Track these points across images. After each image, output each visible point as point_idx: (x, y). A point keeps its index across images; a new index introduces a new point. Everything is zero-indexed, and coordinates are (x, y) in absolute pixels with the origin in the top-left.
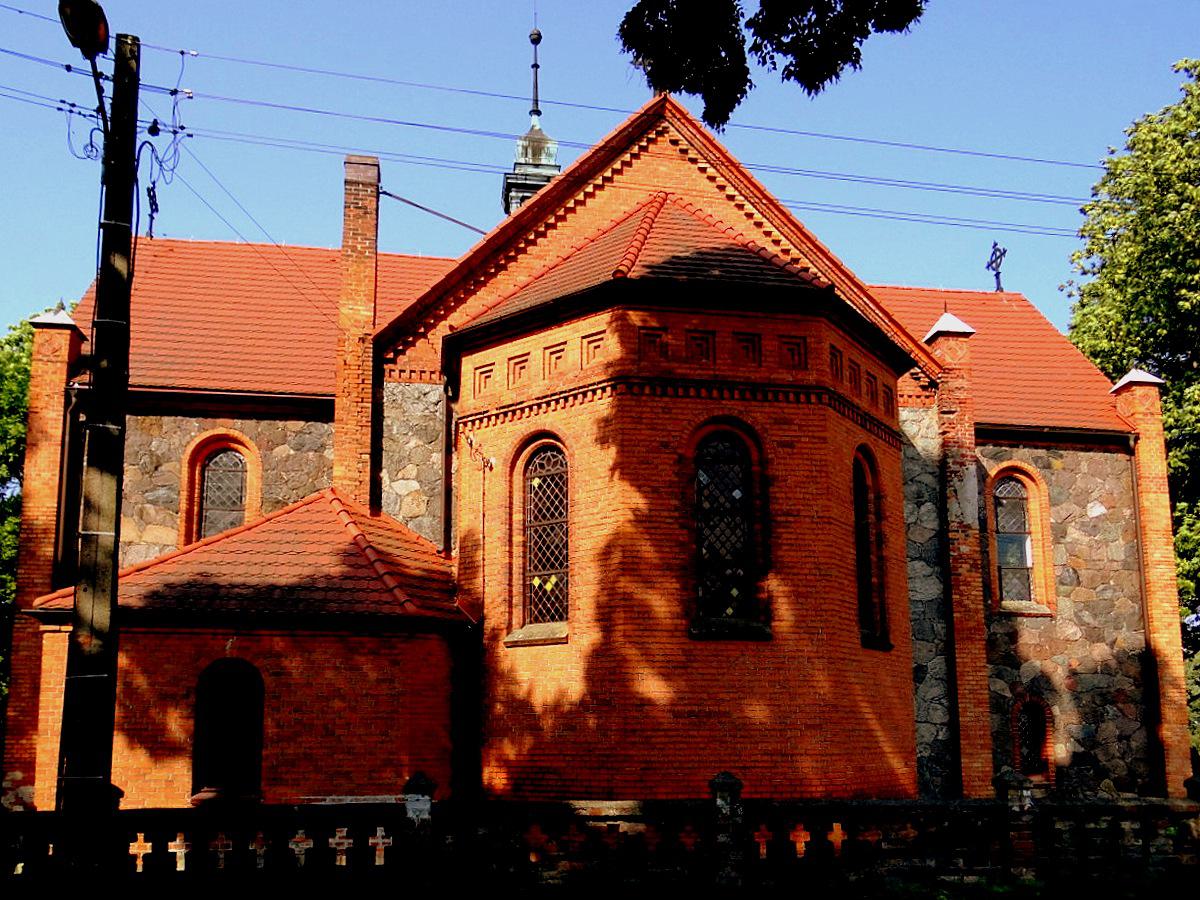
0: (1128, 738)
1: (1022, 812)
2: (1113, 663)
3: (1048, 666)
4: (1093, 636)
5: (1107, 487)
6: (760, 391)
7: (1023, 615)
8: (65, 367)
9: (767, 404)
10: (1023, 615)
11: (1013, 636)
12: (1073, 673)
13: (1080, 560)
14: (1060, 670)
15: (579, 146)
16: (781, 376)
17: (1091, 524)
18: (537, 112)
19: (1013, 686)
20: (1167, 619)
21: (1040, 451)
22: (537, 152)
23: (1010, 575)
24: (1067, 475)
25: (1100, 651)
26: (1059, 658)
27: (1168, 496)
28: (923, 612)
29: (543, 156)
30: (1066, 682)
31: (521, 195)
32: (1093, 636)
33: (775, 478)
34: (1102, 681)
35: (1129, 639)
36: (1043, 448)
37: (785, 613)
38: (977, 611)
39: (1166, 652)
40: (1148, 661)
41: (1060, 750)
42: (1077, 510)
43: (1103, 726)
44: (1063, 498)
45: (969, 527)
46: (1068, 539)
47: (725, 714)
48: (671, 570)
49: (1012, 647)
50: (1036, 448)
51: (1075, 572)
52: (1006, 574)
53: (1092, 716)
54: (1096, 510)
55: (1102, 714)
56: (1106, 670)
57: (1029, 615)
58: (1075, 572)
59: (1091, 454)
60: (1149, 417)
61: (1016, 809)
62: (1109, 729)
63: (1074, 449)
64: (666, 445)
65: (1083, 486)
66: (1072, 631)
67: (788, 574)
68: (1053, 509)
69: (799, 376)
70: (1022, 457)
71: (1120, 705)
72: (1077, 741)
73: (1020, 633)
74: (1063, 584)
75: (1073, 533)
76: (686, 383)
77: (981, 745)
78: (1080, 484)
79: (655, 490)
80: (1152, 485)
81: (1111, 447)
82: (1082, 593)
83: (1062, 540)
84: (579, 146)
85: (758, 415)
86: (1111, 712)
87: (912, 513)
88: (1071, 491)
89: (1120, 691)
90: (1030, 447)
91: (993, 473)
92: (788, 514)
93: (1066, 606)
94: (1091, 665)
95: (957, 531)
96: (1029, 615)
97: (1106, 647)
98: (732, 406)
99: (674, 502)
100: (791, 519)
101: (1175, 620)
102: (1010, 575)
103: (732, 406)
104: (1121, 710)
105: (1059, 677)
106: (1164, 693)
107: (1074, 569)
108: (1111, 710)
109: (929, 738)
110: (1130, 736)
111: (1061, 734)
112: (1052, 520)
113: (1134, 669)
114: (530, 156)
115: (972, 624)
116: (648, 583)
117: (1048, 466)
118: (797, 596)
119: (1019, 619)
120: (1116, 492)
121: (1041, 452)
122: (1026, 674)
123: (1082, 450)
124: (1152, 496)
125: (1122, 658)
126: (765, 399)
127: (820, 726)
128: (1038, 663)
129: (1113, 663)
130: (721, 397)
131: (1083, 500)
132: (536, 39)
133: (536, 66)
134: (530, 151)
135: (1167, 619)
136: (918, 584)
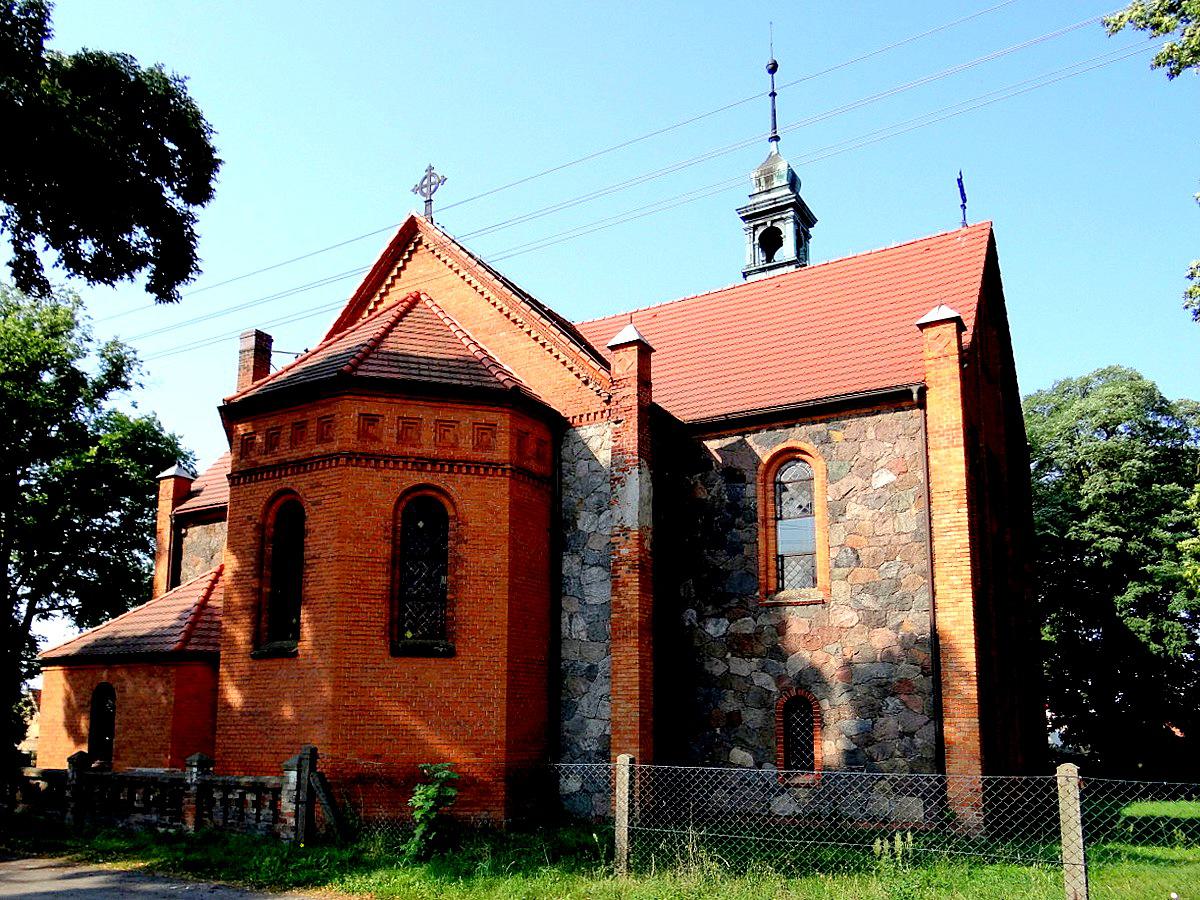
0: (911, 734)
1: (192, 784)
2: (897, 650)
3: (818, 658)
4: (873, 620)
5: (897, 450)
6: (300, 466)
7: (790, 604)
8: (171, 502)
9: (307, 475)
10: (790, 604)
11: (781, 629)
12: (848, 664)
13: (862, 538)
14: (832, 661)
15: (340, 277)
16: (316, 451)
17: (876, 496)
18: (776, 139)
19: (779, 679)
20: (954, 594)
21: (819, 425)
22: (768, 180)
23: (794, 563)
24: (849, 446)
25: (882, 639)
26: (832, 648)
27: (962, 449)
28: (598, 615)
29: (775, 179)
30: (839, 673)
31: (752, 225)
32: (873, 620)
33: (309, 531)
34: (882, 671)
35: (915, 623)
36: (821, 422)
37: (307, 631)
38: (632, 611)
39: (953, 633)
40: (935, 642)
41: (829, 748)
42: (859, 482)
43: (881, 720)
44: (844, 471)
45: (628, 529)
46: (848, 516)
47: (270, 713)
48: (246, 609)
49: (779, 638)
50: (814, 423)
51: (854, 551)
52: (789, 563)
53: (868, 711)
54: (883, 478)
55: (880, 709)
56: (889, 658)
57: (797, 604)
58: (854, 551)
59: (879, 417)
60: (942, 360)
61: (189, 781)
62: (889, 724)
63: (859, 416)
64: (250, 518)
65: (868, 455)
66: (847, 617)
67: (311, 604)
68: (830, 486)
69: (328, 447)
70: (798, 436)
71: (904, 697)
72: (850, 737)
73: (789, 624)
74: (837, 566)
75: (854, 509)
76: (265, 469)
77: (630, 739)
78: (865, 453)
79: (243, 553)
80: (942, 439)
81: (903, 404)
82: (862, 574)
83: (840, 519)
84: (340, 277)
85: (300, 483)
86: (891, 705)
87: (592, 523)
88: (853, 463)
89: (904, 682)
90: (807, 423)
91: (765, 459)
92: (314, 557)
93: (841, 589)
94: (869, 654)
95: (619, 535)
96: (797, 604)
97: (889, 632)
98: (287, 482)
99: (252, 559)
100: (315, 561)
101: (964, 595)
102: (794, 563)
103: (287, 482)
104: (904, 703)
105: (832, 668)
106: (947, 683)
107: (852, 548)
108: (892, 703)
109: (596, 733)
110: (914, 733)
111: (832, 730)
112: (830, 499)
113: (923, 655)
114: (763, 184)
115: (627, 623)
116: (235, 620)
117: (827, 440)
118: (314, 620)
119: (788, 609)
120: (908, 454)
121: (821, 427)
122: (793, 667)
123: (867, 415)
124: (943, 452)
125: (909, 644)
126: (305, 471)
127: (321, 721)
128: (806, 655)
129: (897, 650)
130: (280, 477)
131: (868, 469)
132: (773, 69)
133: (773, 94)
134: (762, 180)
135: (954, 594)
136: (594, 590)
